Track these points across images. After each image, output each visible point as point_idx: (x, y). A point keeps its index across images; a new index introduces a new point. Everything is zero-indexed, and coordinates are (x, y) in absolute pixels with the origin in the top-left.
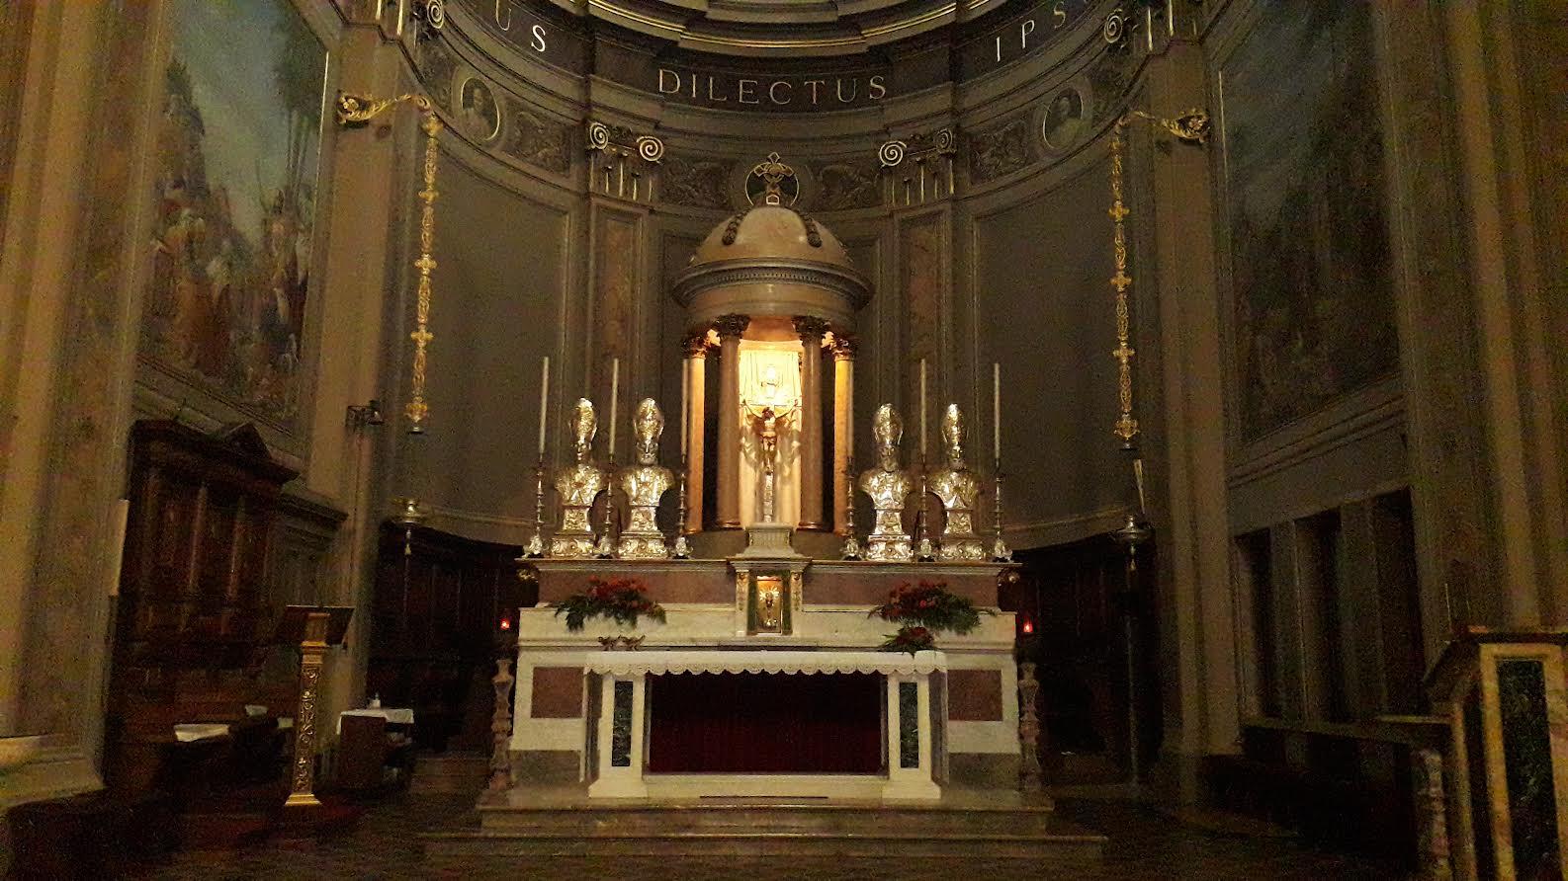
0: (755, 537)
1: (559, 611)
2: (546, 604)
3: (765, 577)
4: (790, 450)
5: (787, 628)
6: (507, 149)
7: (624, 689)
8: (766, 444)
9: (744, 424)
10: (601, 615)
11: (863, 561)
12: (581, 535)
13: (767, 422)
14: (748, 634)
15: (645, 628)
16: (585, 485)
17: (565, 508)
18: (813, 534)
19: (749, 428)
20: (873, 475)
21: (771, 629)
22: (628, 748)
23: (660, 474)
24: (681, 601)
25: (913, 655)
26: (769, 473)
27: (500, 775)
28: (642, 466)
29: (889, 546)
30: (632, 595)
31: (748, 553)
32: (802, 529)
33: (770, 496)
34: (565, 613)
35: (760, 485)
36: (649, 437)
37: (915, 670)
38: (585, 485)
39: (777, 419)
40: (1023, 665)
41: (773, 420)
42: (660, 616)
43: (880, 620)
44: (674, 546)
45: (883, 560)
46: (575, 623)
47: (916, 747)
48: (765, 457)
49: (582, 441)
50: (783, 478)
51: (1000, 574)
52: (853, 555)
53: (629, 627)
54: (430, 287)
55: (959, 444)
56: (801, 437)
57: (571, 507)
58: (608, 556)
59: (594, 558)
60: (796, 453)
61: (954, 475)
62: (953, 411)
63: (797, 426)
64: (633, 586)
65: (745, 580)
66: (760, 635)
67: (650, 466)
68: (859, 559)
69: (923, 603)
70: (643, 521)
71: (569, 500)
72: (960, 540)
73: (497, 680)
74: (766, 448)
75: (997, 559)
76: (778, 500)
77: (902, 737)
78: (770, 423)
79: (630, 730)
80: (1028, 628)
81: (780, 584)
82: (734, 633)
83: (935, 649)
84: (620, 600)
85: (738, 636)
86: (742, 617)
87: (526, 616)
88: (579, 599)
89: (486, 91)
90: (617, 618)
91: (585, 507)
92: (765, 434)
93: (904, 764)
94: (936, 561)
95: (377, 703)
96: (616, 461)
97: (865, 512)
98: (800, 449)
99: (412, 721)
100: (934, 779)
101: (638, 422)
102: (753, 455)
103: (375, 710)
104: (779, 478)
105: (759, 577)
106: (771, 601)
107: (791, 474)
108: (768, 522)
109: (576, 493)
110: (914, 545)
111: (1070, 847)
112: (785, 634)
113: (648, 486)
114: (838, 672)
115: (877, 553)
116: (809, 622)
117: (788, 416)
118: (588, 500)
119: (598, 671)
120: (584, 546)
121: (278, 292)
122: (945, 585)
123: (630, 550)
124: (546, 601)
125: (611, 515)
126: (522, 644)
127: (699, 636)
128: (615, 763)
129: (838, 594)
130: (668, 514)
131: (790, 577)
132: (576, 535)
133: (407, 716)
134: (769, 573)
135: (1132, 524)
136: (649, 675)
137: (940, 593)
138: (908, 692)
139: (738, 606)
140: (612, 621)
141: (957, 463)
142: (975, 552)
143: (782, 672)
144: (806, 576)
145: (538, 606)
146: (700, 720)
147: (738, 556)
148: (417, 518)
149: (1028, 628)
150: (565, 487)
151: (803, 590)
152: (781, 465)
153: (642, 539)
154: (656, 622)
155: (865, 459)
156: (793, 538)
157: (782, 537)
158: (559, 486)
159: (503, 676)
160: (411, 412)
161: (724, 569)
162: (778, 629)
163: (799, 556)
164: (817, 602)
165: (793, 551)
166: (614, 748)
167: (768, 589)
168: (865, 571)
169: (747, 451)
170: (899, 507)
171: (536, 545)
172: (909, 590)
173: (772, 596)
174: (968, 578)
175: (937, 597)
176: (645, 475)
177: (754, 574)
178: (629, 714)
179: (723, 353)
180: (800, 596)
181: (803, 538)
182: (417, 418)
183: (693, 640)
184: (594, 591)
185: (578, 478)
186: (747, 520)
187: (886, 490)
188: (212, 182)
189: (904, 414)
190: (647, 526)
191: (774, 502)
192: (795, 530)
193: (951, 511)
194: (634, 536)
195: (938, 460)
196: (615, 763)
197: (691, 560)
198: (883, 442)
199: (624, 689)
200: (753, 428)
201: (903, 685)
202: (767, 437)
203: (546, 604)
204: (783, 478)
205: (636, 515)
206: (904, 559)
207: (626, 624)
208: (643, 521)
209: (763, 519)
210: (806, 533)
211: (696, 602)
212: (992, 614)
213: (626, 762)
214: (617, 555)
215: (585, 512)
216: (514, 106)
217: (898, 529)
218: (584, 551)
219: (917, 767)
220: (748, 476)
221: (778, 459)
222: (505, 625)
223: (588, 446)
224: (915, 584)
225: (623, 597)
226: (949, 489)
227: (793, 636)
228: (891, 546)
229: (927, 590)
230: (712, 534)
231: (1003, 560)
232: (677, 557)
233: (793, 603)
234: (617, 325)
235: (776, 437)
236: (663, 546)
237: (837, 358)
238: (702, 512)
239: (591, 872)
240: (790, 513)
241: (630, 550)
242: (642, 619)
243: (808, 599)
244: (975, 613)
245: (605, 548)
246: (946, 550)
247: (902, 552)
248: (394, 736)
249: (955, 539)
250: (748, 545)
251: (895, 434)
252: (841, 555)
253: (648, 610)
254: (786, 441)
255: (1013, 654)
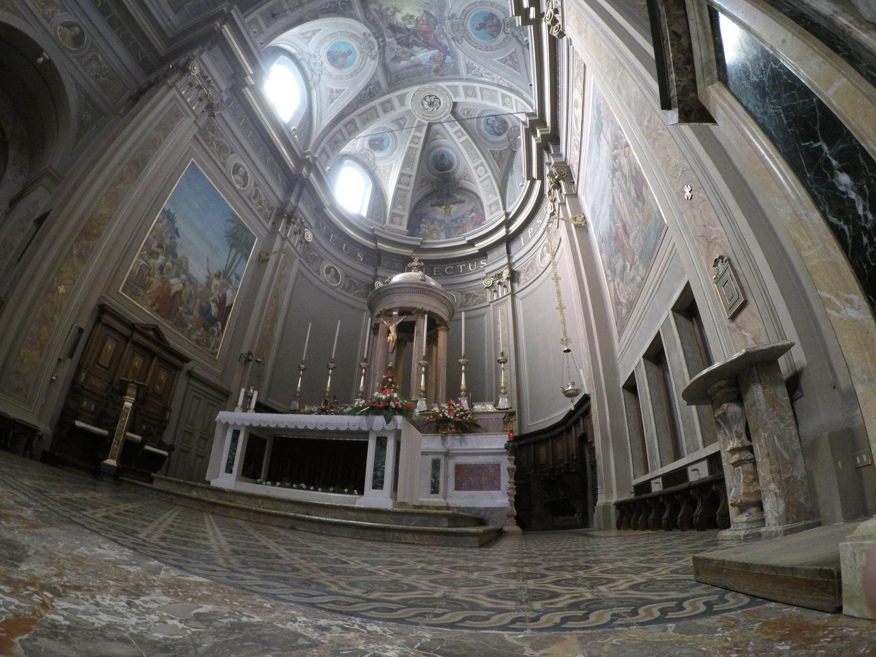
6: (343, 289)
89: (336, 271)
93: (375, 487)
111: (638, 278)
121: (213, 305)
128: (226, 472)
178: (237, 443)
188: (180, 252)
196: (226, 472)
216: (347, 276)
239: (471, 572)
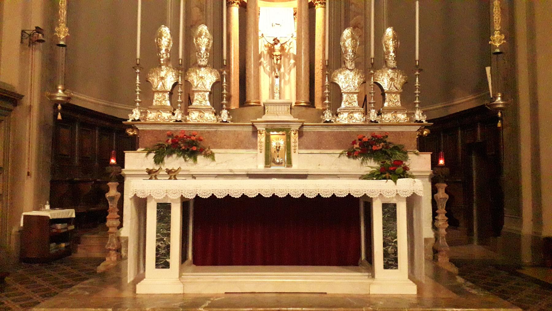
0: (269, 109)
1: (148, 154)
2: (143, 149)
3: (275, 133)
4: (289, 64)
5: (289, 163)
7: (164, 209)
8: (275, 59)
9: (263, 50)
10: (175, 156)
11: (335, 123)
12: (163, 108)
13: (276, 46)
14: (265, 167)
15: (202, 164)
16: (167, 78)
17: (154, 92)
18: (304, 109)
19: (266, 52)
20: (340, 72)
21: (279, 164)
22: (168, 253)
23: (211, 72)
24: (225, 148)
25: (395, 182)
26: (277, 77)
27: (112, 253)
28: (200, 67)
29: (350, 116)
30: (193, 143)
31: (264, 118)
32: (298, 105)
33: (278, 89)
34: (152, 155)
35: (272, 86)
36: (203, 49)
37: (397, 194)
38: (167, 78)
39: (281, 45)
40: (437, 185)
41: (279, 45)
42: (211, 156)
43: (347, 158)
44: (220, 115)
45: (346, 122)
46: (158, 160)
47: (396, 253)
48: (275, 68)
49: (163, 51)
50: (285, 81)
51: (418, 130)
52: (328, 120)
53: (192, 162)
54: (213, 106)
55: (394, 52)
56: (297, 58)
57: (158, 92)
58: (180, 121)
59: (171, 122)
60: (292, 66)
61: (390, 71)
62: (389, 32)
63: (294, 51)
64: (193, 138)
65: (263, 135)
66: (272, 168)
67: (205, 66)
68: (332, 122)
69: (374, 148)
70: (201, 100)
71: (157, 87)
72: (395, 110)
73: (107, 195)
74: (275, 62)
75: (417, 121)
76: (282, 92)
77: (385, 245)
78: (277, 47)
79: (169, 241)
80: (441, 162)
81: (285, 137)
82: (257, 166)
83: (413, 177)
84: (185, 146)
85: (259, 168)
86: (262, 157)
87: (129, 156)
88: (161, 146)
90: (184, 157)
91: (166, 92)
92: (274, 54)
93: (387, 266)
94: (379, 123)
95: (48, 207)
96: (185, 65)
97: (336, 95)
98: (295, 64)
99: (74, 216)
100: (410, 278)
101: (196, 39)
102: (268, 68)
103: (47, 212)
104: (283, 81)
105: (271, 133)
106: (279, 147)
107: (289, 80)
108: (277, 100)
109: (161, 83)
110: (366, 113)
112: (288, 167)
113: (204, 79)
114: (334, 195)
115: (343, 118)
116: (301, 161)
117: (288, 43)
118: (169, 86)
119: (140, 195)
120: (166, 115)
122: (387, 136)
123: (194, 117)
124: (142, 148)
125: (183, 96)
126: (126, 173)
127: (236, 168)
129: (320, 143)
130: (217, 96)
131: (290, 133)
132: (163, 108)
133: (71, 213)
134: (278, 130)
135: (499, 99)
136: (182, 197)
137: (385, 142)
138: (390, 210)
139: (259, 150)
140: (182, 159)
141: (392, 64)
142: (402, 117)
143: (289, 196)
144: (301, 133)
145: (139, 150)
146: (226, 231)
147: (258, 120)
148: (63, 97)
149: (441, 162)
150: (155, 81)
151: (299, 141)
152: (284, 74)
153: (200, 110)
154: (209, 160)
155: (336, 61)
156: (292, 110)
157: (286, 108)
158: (150, 79)
159: (113, 192)
160: (59, 32)
161: (250, 129)
162: (284, 164)
163: (297, 119)
164: (307, 148)
165: (292, 117)
166: (157, 254)
167: (277, 140)
168: (335, 129)
169: (265, 65)
170: (357, 91)
171: (136, 114)
172: (365, 139)
173: (279, 144)
174: (399, 133)
175: (383, 144)
176: (203, 72)
177: (268, 130)
179: (248, 6)
180: (297, 144)
181: (298, 110)
182: (62, 37)
183: (231, 171)
184: (170, 141)
185: (162, 74)
186: (265, 97)
187: (348, 80)
189: (361, 31)
190: (204, 103)
191: (280, 93)
192: (293, 104)
193: (388, 92)
194: (196, 109)
195: (379, 63)
197: (230, 123)
198: (346, 52)
199: (164, 209)
200: (268, 53)
201: (385, 206)
202: (276, 55)
203: (143, 149)
204: (285, 81)
205: (197, 96)
206: (358, 122)
207: (191, 161)
208: (201, 100)
209: (273, 98)
210: (299, 107)
211: (235, 148)
212: (417, 154)
213: (167, 265)
214: (186, 120)
215: (167, 95)
217: (356, 104)
218: (166, 118)
219: (397, 268)
220: (265, 80)
221: (282, 70)
222: (113, 161)
223: (167, 55)
224: (368, 137)
225: (190, 146)
226: (386, 79)
227: (293, 168)
228: (351, 115)
229: (376, 139)
230: (245, 108)
231: (420, 121)
232: (223, 121)
233: (292, 148)
234: (198, 10)
235: (281, 55)
236: (214, 115)
237: (316, 6)
238: (236, 96)
240: (290, 94)
241: (194, 117)
242: (200, 158)
243: (301, 146)
244: (406, 153)
245: (178, 116)
246: (385, 116)
247: (358, 117)
248: (59, 226)
249: (389, 110)
250: (264, 113)
251: (354, 47)
252: (320, 120)
253: (203, 153)
254: (287, 60)
255: (429, 178)
